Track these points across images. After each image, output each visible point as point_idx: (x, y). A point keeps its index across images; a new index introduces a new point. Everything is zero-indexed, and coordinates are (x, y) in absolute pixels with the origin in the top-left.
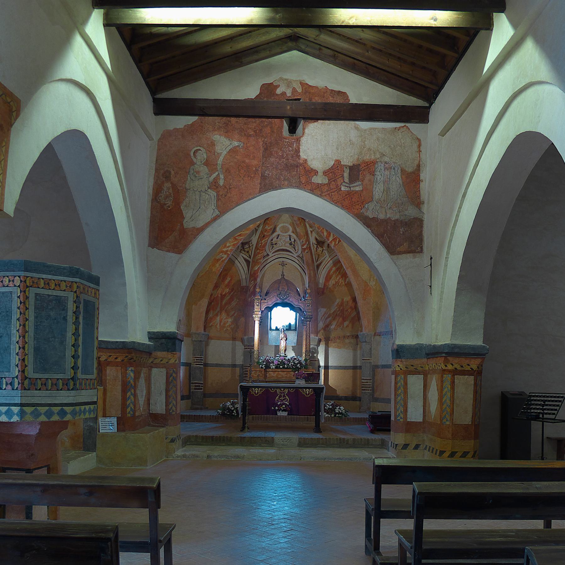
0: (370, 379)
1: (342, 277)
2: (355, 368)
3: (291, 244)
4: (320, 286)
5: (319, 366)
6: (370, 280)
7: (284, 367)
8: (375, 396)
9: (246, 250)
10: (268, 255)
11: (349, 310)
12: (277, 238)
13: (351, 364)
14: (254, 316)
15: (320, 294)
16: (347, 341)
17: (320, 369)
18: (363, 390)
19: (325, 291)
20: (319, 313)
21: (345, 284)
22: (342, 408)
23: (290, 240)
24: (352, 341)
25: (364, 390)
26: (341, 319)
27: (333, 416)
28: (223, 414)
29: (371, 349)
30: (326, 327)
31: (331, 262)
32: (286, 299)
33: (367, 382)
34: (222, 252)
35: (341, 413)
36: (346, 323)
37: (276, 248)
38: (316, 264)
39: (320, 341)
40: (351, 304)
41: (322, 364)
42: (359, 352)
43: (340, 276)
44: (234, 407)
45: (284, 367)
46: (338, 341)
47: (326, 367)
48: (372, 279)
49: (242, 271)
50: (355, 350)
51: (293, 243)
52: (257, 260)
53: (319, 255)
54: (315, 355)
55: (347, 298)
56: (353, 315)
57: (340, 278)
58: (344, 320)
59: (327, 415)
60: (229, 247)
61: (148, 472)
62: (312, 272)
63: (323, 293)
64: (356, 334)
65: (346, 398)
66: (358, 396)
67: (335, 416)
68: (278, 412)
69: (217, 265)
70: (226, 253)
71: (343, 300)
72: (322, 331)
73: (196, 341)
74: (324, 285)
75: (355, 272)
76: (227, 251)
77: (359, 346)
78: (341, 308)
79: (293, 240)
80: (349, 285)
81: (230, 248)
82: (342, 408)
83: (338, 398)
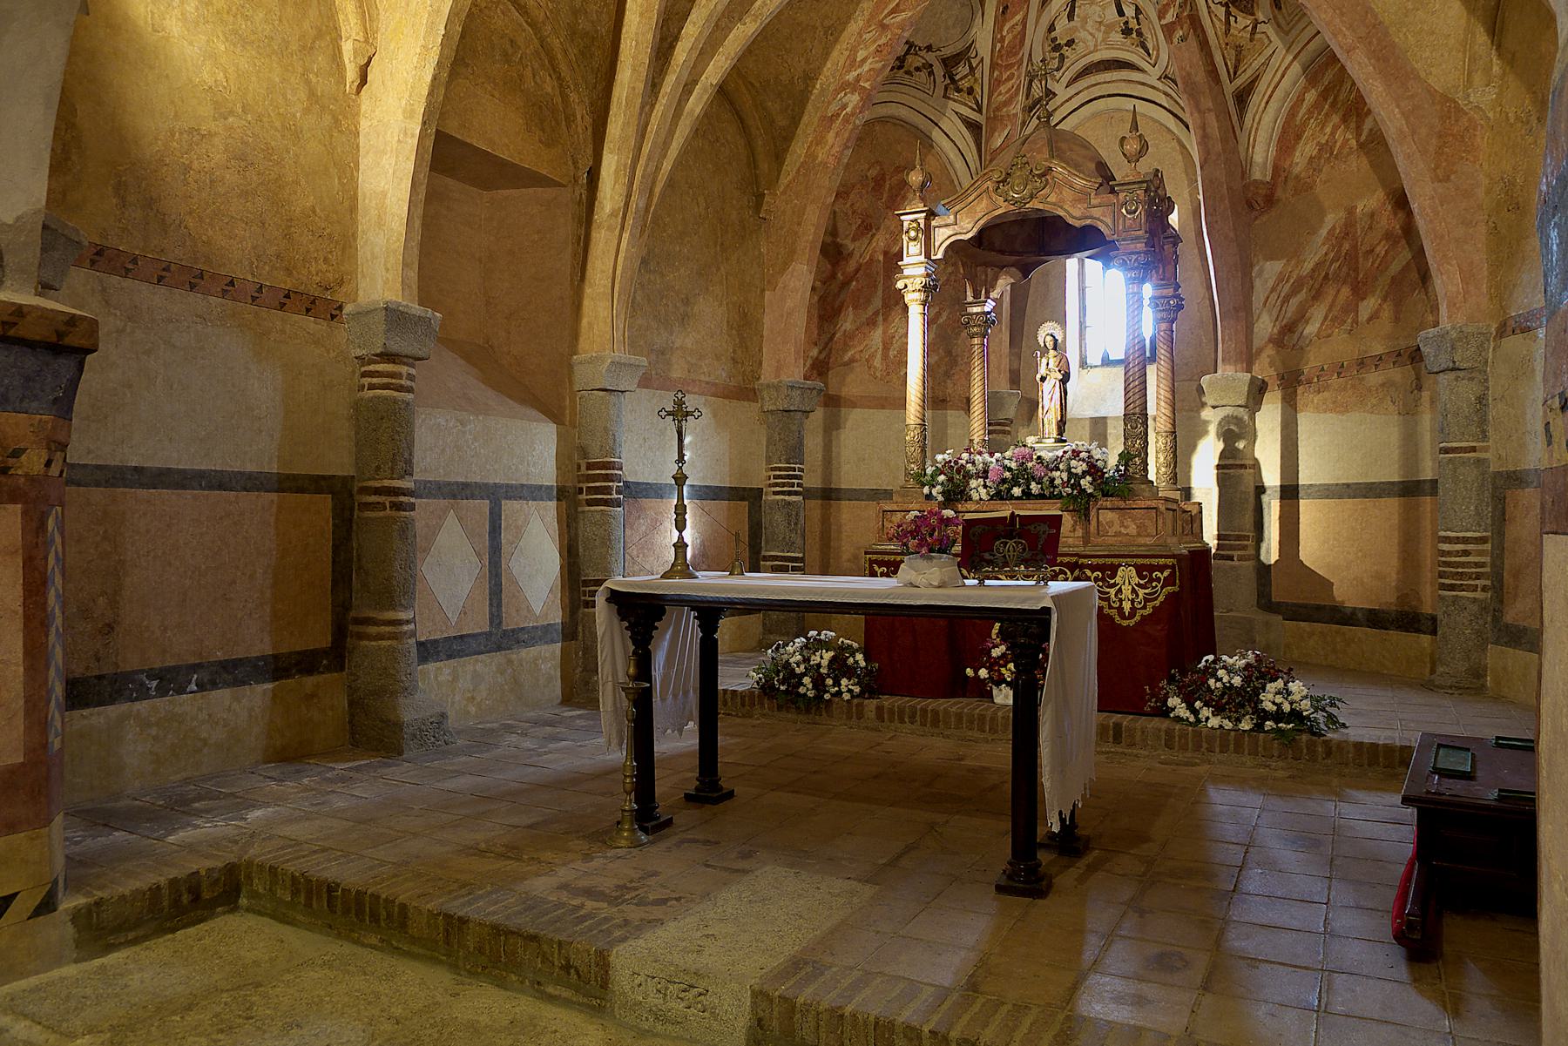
0: (1483, 540)
1: (1345, 120)
2: (1410, 489)
3: (1127, 31)
4: (1257, 175)
5: (1261, 489)
6: (1469, 82)
7: (1027, 494)
8: (1509, 617)
9: (965, 84)
10: (1050, 94)
11: (1381, 250)
12: (1071, 17)
13: (1391, 473)
14: (900, 285)
15: (1252, 208)
16: (1374, 378)
17: (1265, 498)
18: (1444, 587)
19: (1279, 193)
20: (1258, 283)
21: (1361, 146)
22: (1295, 686)
23: (1121, 13)
24: (1396, 374)
25: (1452, 588)
26: (1346, 291)
27: (1246, 725)
28: (767, 689)
29: (1481, 400)
30: (1287, 334)
31: (1296, 68)
32: (1032, 197)
33: (1466, 553)
34: (844, 86)
35: (1296, 715)
36: (1368, 306)
37: (1076, 60)
38: (1229, 88)
39: (1258, 392)
40: (1388, 221)
41: (1272, 477)
42: (1426, 421)
43: (1336, 119)
44: (806, 660)
45: (1027, 494)
46: (1334, 380)
47: (1290, 492)
48: (1478, 78)
49: (959, 164)
50: (1409, 412)
51: (1133, 24)
52: (998, 109)
53: (1239, 49)
54: (1241, 445)
55: (1372, 201)
56: (1395, 267)
57: (1335, 128)
58: (1359, 292)
59: (1214, 722)
60: (864, 61)
61: (1260, 617)
62: (1212, 119)
63: (1270, 200)
64: (1412, 343)
65: (1375, 619)
66: (1427, 608)
67: (1259, 727)
68: (995, 691)
69: (831, 137)
70: (854, 86)
71: (1351, 211)
72: (1270, 351)
73: (772, 412)
74: (1276, 168)
75: (1389, 59)
76: (858, 79)
77: (1426, 394)
78: (1346, 246)
79: (1129, 12)
80: (1375, 146)
81: (866, 67)
82: (1295, 686)
83: (1341, 616)
